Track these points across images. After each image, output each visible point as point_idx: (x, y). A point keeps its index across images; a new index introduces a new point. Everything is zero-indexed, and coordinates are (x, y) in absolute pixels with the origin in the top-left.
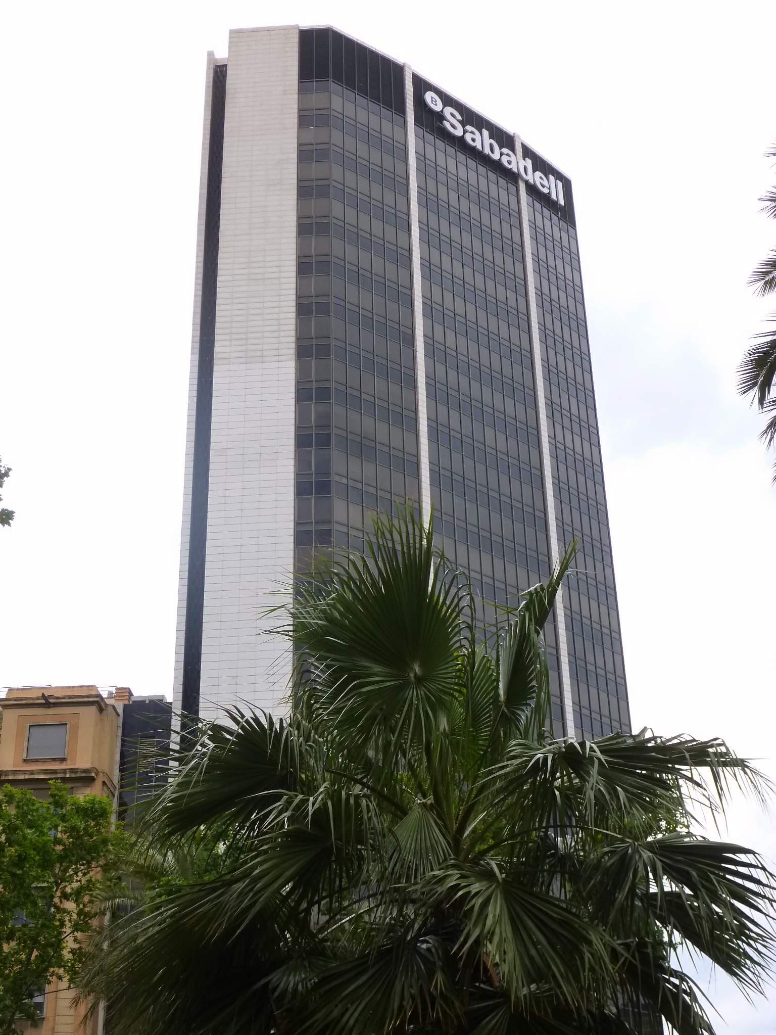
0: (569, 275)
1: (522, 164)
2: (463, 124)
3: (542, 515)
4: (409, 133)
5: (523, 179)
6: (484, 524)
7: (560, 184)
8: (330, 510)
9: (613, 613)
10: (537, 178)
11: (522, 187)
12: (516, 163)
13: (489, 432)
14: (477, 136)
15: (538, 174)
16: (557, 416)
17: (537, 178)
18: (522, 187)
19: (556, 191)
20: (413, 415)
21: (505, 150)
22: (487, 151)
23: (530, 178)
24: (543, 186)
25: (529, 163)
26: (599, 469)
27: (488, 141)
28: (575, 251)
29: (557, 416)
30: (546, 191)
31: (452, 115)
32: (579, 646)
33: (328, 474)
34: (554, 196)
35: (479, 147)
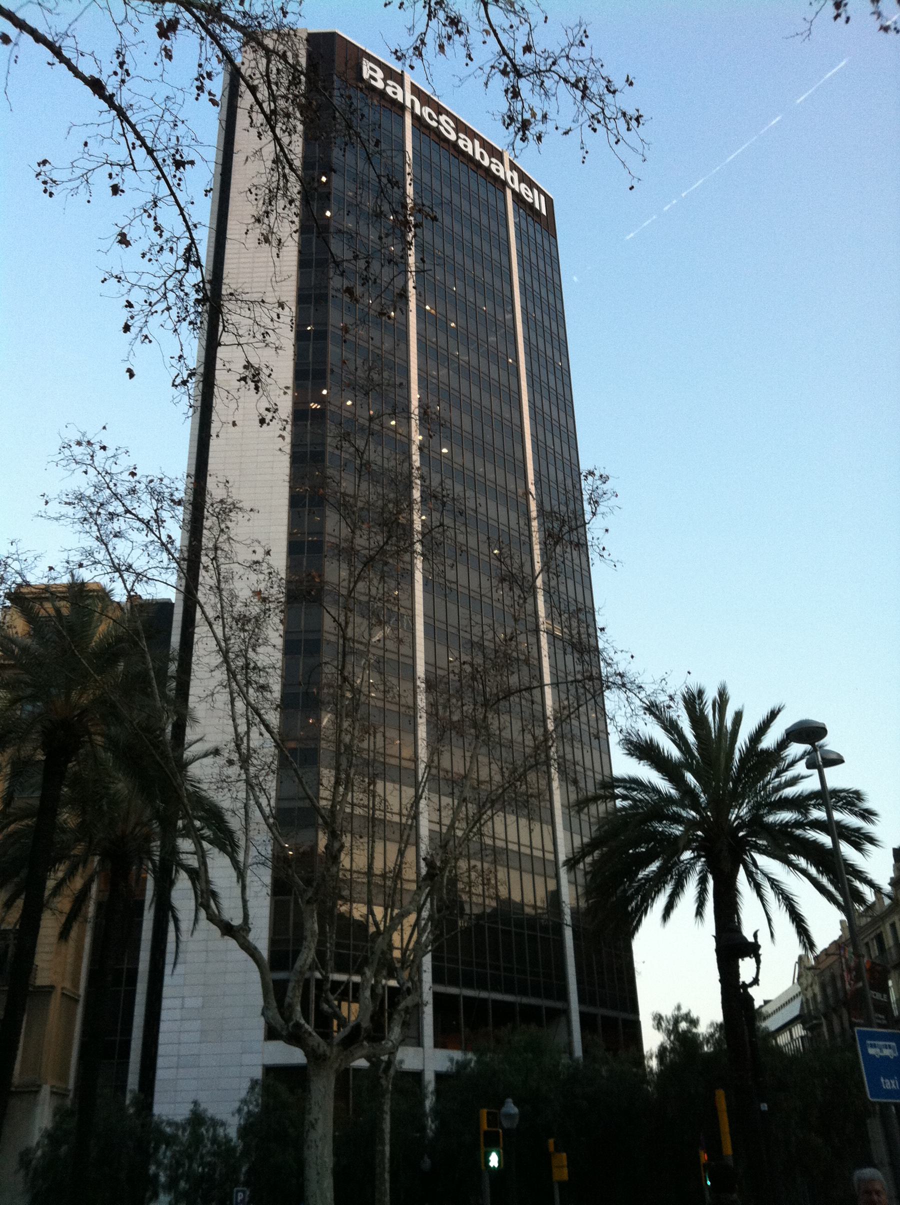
0: (563, 422)
1: (509, 174)
2: (457, 131)
3: (522, 465)
4: (417, 639)
5: (510, 187)
6: (474, 586)
7: (543, 198)
8: (322, 523)
9: (587, 592)
10: (523, 188)
11: (509, 193)
12: (503, 172)
13: (482, 500)
14: (469, 144)
15: (523, 186)
16: (537, 386)
17: (523, 188)
18: (509, 193)
19: (540, 205)
20: (410, 662)
21: (494, 160)
22: (478, 157)
23: (516, 186)
24: (528, 196)
25: (515, 175)
26: (587, 574)
27: (478, 150)
28: (563, 338)
29: (537, 386)
30: (530, 200)
31: (447, 122)
32: (528, 280)
33: (326, 324)
34: (537, 206)
35: (471, 153)
